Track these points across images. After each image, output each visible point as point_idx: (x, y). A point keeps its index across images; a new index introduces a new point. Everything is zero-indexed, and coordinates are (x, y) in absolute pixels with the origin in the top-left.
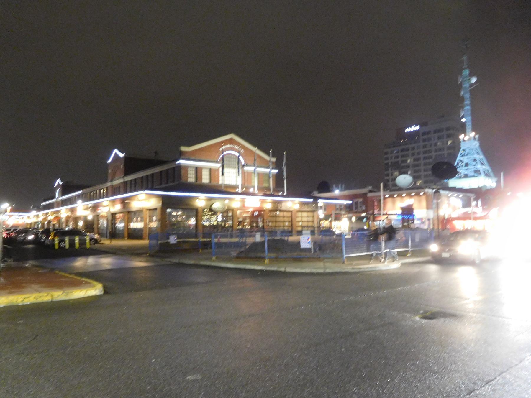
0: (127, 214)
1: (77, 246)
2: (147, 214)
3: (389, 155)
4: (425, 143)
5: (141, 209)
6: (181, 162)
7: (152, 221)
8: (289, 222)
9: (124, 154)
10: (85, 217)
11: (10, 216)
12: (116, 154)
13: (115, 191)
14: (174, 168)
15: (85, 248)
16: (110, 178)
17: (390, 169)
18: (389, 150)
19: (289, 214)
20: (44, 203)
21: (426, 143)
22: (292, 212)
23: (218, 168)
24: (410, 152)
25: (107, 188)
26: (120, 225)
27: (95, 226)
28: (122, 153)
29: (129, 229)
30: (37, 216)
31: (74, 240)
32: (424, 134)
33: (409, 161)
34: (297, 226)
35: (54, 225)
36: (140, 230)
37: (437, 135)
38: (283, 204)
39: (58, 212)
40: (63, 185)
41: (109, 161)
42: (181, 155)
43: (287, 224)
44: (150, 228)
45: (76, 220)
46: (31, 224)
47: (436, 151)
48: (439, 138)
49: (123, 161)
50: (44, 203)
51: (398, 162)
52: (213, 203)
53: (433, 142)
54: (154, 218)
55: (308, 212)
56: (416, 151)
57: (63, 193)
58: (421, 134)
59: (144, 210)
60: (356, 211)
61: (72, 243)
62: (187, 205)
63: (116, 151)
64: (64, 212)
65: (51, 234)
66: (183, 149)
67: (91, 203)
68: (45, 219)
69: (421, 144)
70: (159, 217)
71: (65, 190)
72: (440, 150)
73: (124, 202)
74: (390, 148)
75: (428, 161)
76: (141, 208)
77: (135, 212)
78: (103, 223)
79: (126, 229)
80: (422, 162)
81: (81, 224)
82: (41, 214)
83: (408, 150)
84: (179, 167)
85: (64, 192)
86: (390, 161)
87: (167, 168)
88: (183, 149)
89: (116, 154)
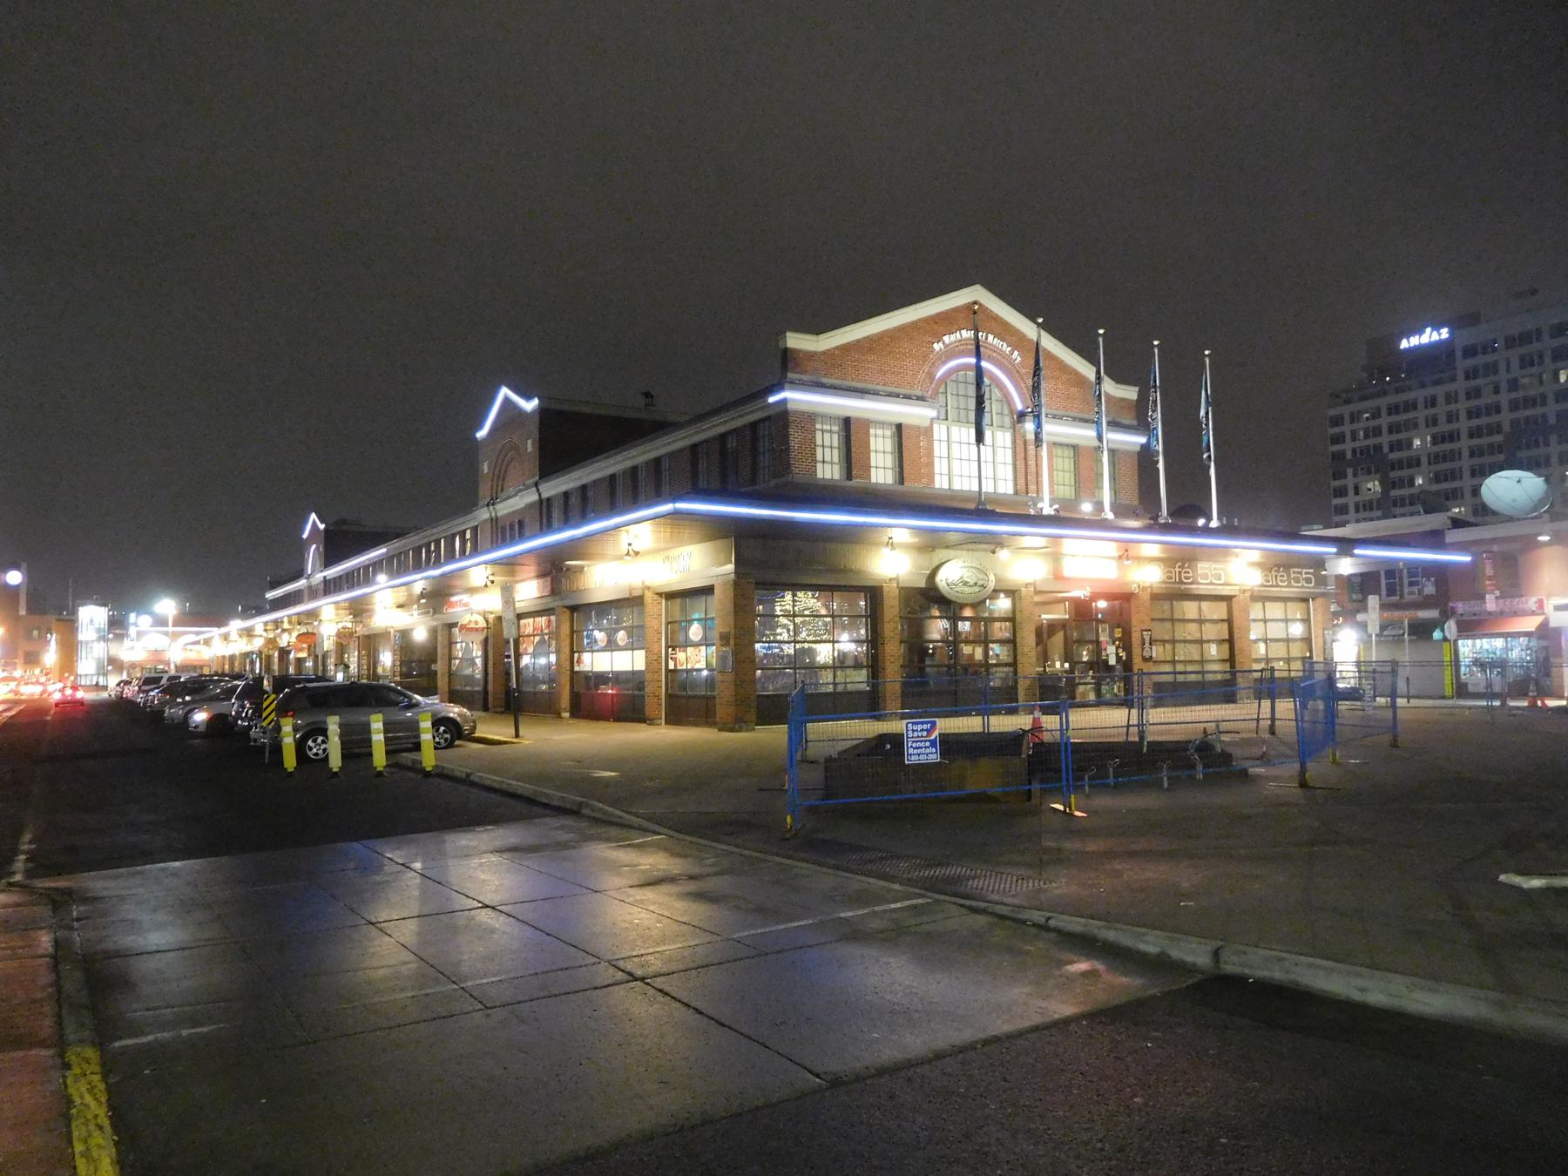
0: (567, 615)
1: (379, 759)
2: (657, 613)
3: (1347, 428)
4: (1473, 383)
5: (637, 593)
6: (795, 398)
7: (687, 644)
8: (1220, 642)
9: (535, 402)
10: (405, 634)
11: (175, 636)
12: (507, 400)
13: (507, 530)
14: (754, 426)
15: (417, 768)
16: (484, 490)
17: (1553, 439)
18: (1346, 410)
19: (1217, 611)
20: (270, 595)
21: (1479, 382)
22: (1228, 599)
23: (927, 423)
24: (1421, 414)
25: (475, 530)
26: (536, 661)
27: (439, 667)
28: (528, 398)
29: (574, 674)
30: (249, 633)
31: (366, 729)
32: (1470, 352)
33: (1417, 442)
34: (1254, 657)
35: (300, 661)
36: (634, 681)
37: (1515, 354)
38: (1203, 567)
39: (313, 615)
40: (326, 530)
41: (481, 434)
42: (786, 366)
43: (1213, 650)
44: (672, 673)
45: (370, 643)
46: (232, 658)
47: (1514, 406)
48: (1526, 362)
49: (534, 428)
50: (270, 595)
51: (1378, 448)
52: (943, 564)
53: (1503, 376)
54: (695, 632)
55: (1285, 600)
56: (1441, 409)
57: (330, 559)
58: (1459, 353)
59: (649, 596)
60: (1395, 599)
61: (356, 746)
62: (845, 571)
63: (505, 392)
64: (331, 619)
65: (273, 706)
66: (796, 341)
67: (419, 582)
68: (271, 642)
69: (1461, 385)
70: (719, 627)
71: (338, 545)
72: (1530, 402)
73: (555, 568)
74: (1348, 402)
75: (1485, 441)
76: (631, 589)
77: (604, 608)
78: (470, 654)
79: (565, 680)
80: (1464, 444)
81: (386, 659)
82: (258, 623)
83: (1414, 406)
84: (782, 418)
85: (332, 555)
86: (1348, 447)
87: (721, 429)
88: (796, 341)
89: (507, 400)
